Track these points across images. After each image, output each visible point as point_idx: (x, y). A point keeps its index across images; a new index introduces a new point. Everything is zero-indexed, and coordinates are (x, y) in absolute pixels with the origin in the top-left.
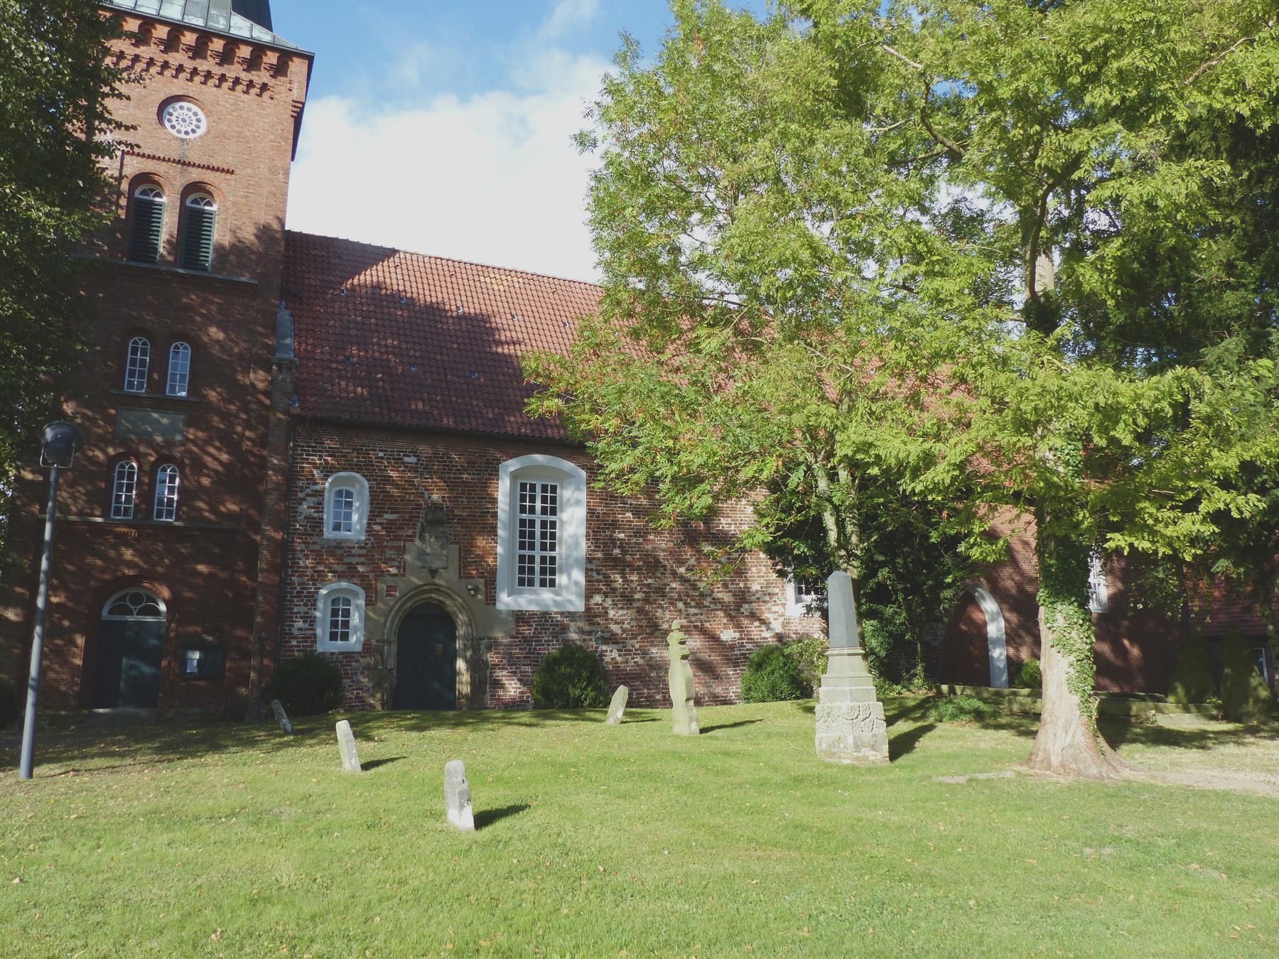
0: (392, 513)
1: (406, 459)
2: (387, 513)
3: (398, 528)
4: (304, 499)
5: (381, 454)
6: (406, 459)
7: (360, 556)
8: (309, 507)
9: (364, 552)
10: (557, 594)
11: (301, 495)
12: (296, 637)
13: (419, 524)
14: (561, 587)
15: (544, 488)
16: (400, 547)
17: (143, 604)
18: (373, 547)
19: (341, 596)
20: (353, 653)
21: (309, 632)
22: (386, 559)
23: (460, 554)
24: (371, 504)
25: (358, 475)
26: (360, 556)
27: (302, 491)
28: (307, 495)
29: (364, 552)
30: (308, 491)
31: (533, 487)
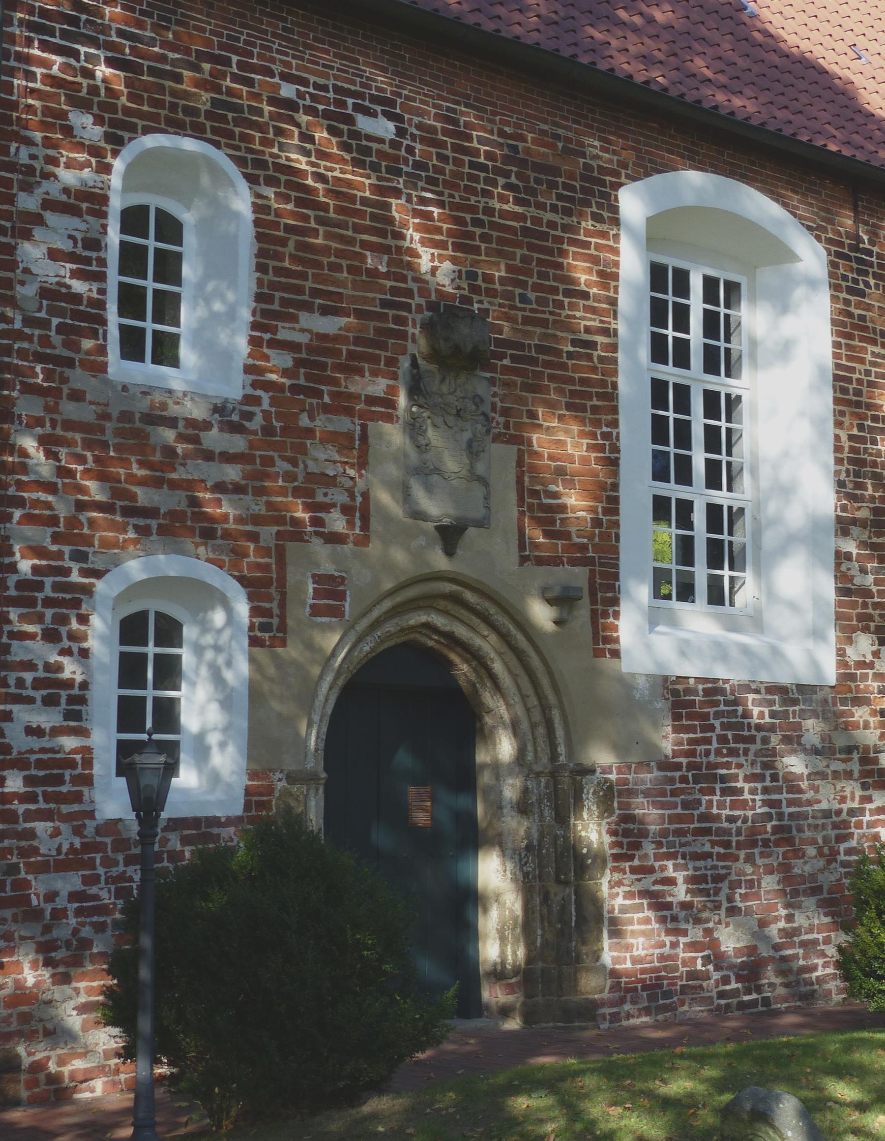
0: (325, 311)
1: (364, 123)
2: (308, 307)
3: (339, 368)
4: (39, 220)
5: (288, 91)
6: (364, 123)
7: (228, 458)
8: (54, 255)
9: (238, 443)
10: (732, 626)
11: (28, 202)
12: (20, 764)
13: (405, 363)
14: (673, 622)
15: (710, 284)
16: (349, 436)
17: (292, 485)
18: (268, 430)
19: (153, 605)
20: (214, 821)
21: (69, 743)
22: (310, 477)
23: (520, 481)
24: (261, 268)
25: (220, 157)
26: (228, 458)
27: (27, 188)
28: (48, 204)
29: (238, 443)
30: (52, 189)
31: (682, 278)
